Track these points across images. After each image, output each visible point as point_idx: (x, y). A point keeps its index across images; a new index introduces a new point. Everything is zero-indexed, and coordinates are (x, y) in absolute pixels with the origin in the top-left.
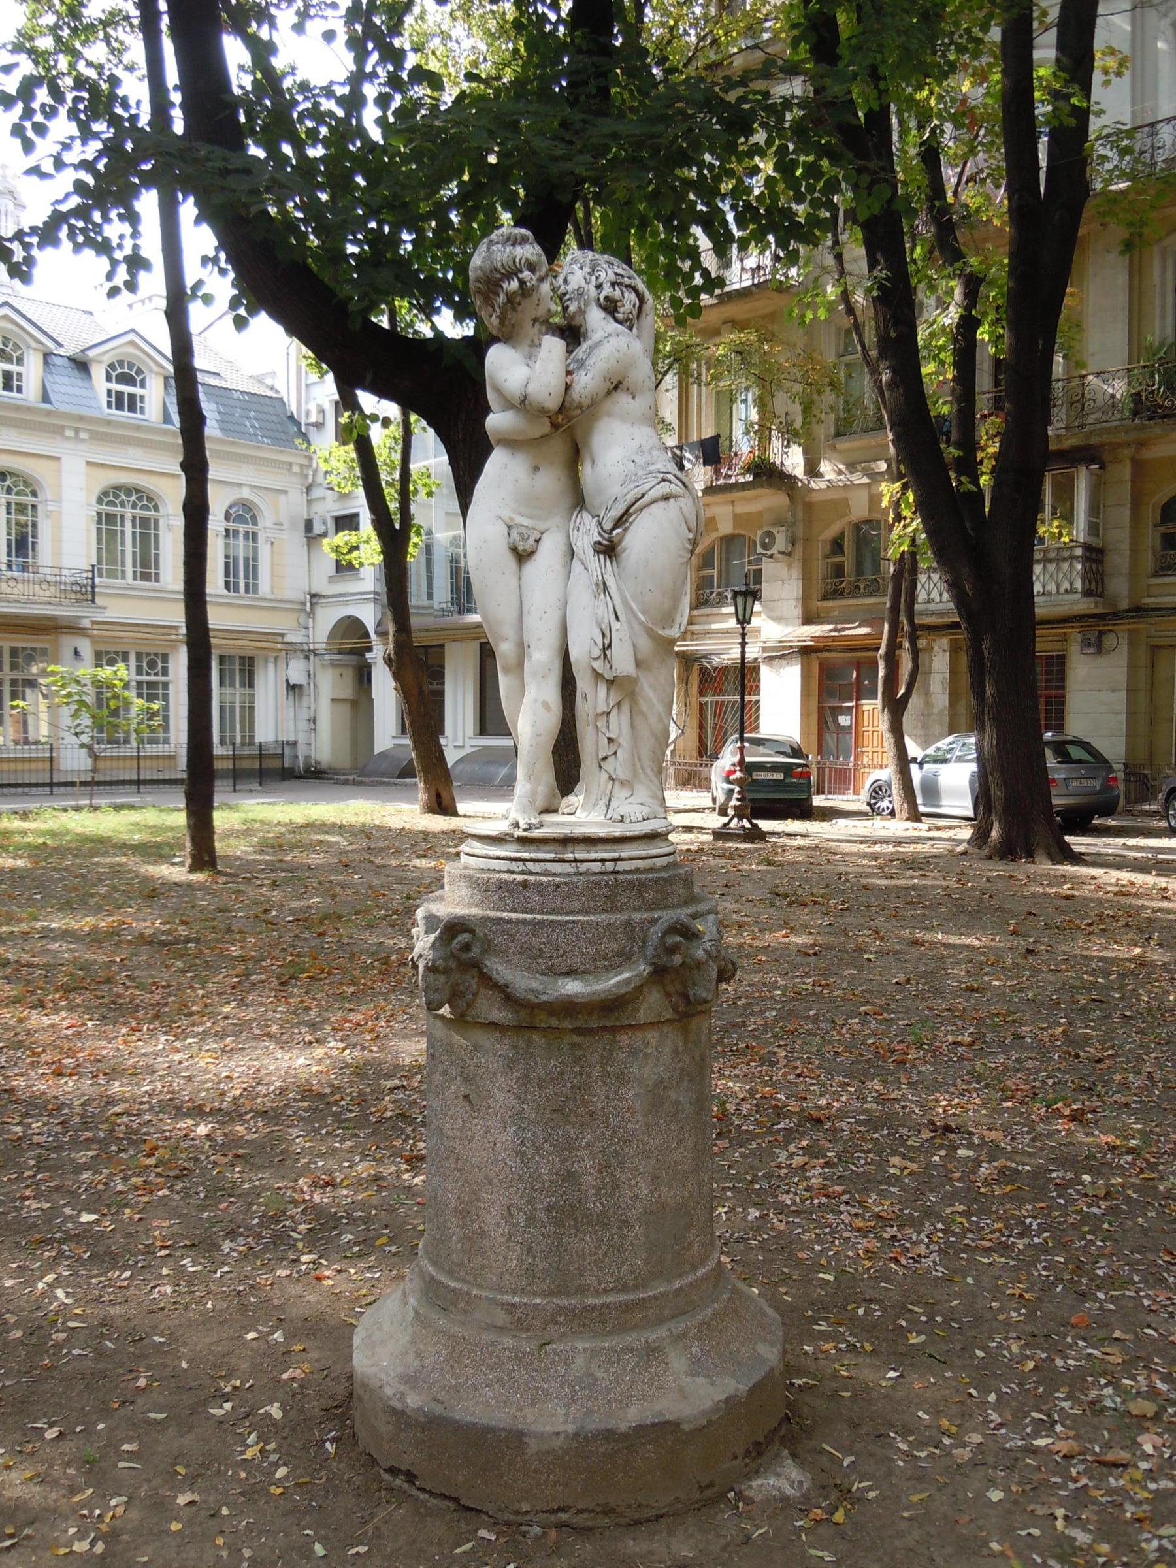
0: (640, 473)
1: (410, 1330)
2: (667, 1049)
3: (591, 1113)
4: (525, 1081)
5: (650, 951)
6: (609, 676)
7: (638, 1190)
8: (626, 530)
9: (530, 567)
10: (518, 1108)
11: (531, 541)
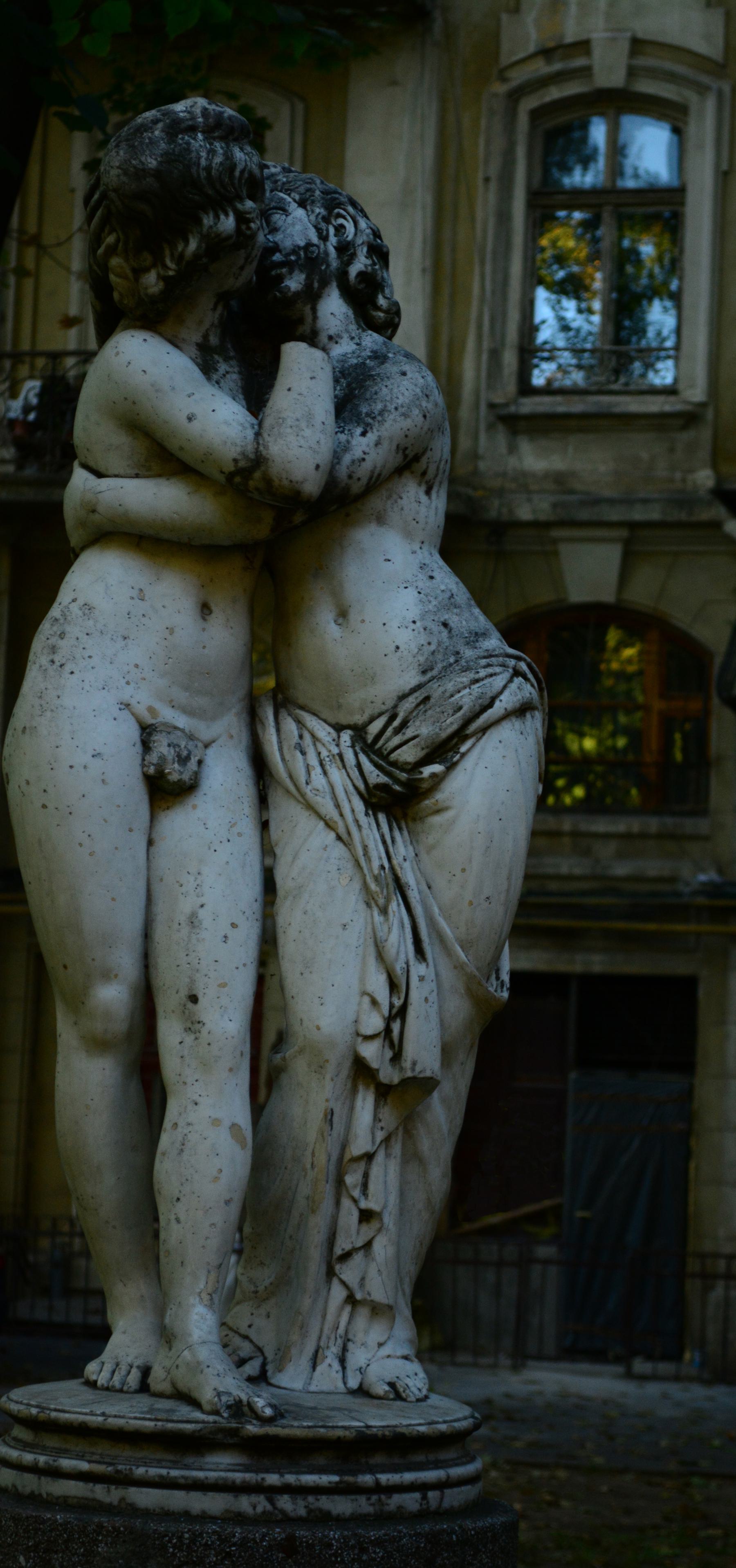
6: (388, 1075)
8: (451, 767)
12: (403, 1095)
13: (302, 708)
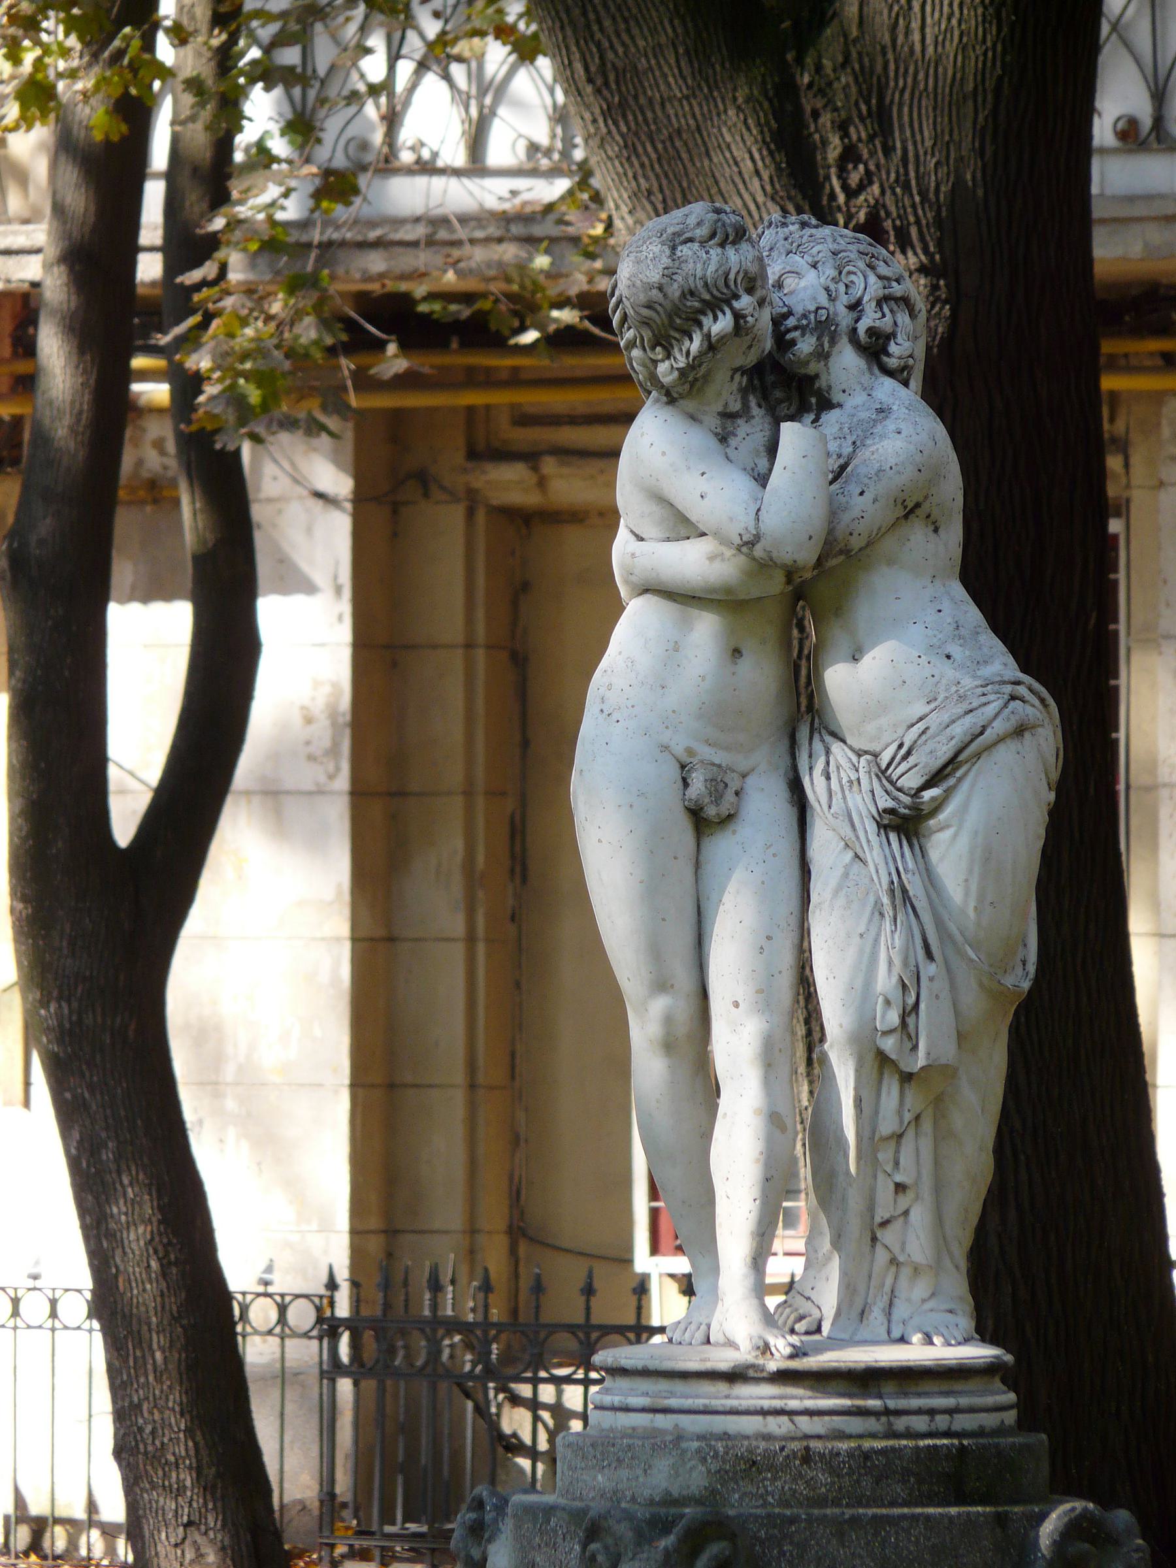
9: (721, 846)
13: (834, 735)
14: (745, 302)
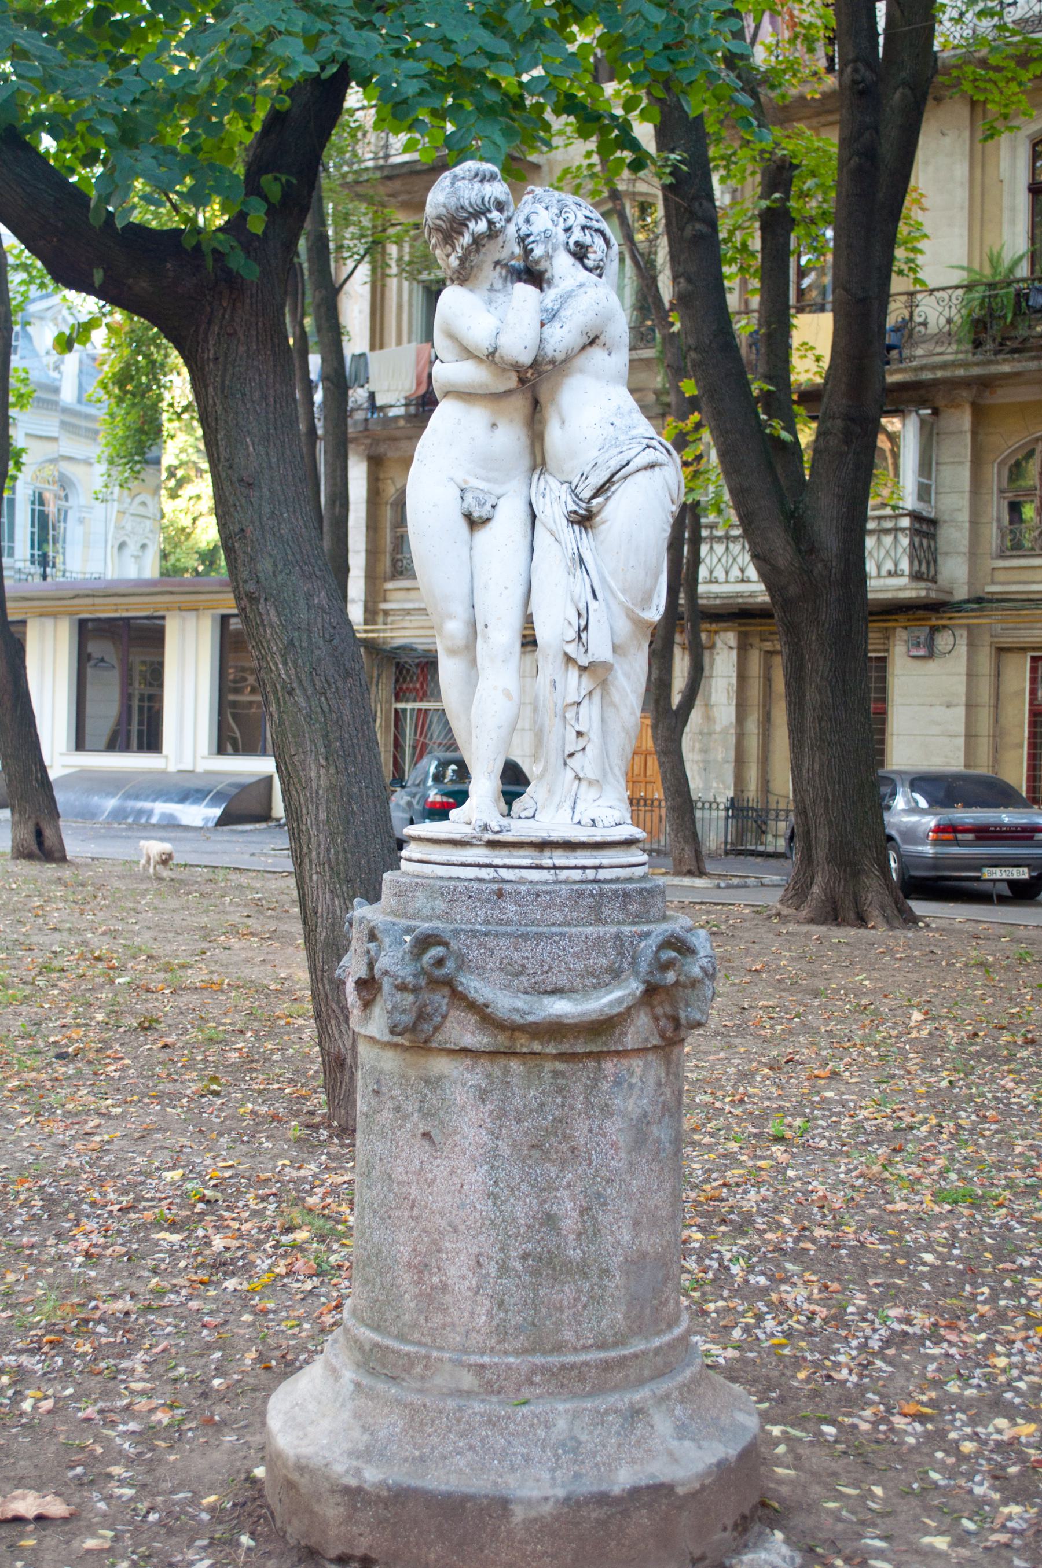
0: (622, 438)
1: (350, 1405)
2: (651, 1080)
3: (573, 1150)
4: (501, 1114)
5: (643, 968)
6: (584, 661)
7: (620, 1236)
8: (607, 499)
9: (483, 535)
10: (491, 1145)
11: (488, 507)
12: (596, 672)
14: (495, 215)
